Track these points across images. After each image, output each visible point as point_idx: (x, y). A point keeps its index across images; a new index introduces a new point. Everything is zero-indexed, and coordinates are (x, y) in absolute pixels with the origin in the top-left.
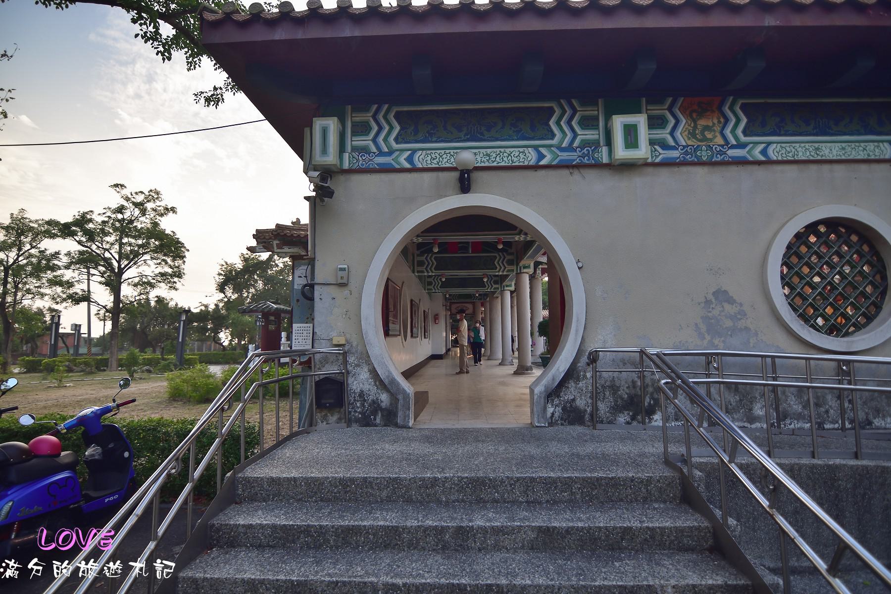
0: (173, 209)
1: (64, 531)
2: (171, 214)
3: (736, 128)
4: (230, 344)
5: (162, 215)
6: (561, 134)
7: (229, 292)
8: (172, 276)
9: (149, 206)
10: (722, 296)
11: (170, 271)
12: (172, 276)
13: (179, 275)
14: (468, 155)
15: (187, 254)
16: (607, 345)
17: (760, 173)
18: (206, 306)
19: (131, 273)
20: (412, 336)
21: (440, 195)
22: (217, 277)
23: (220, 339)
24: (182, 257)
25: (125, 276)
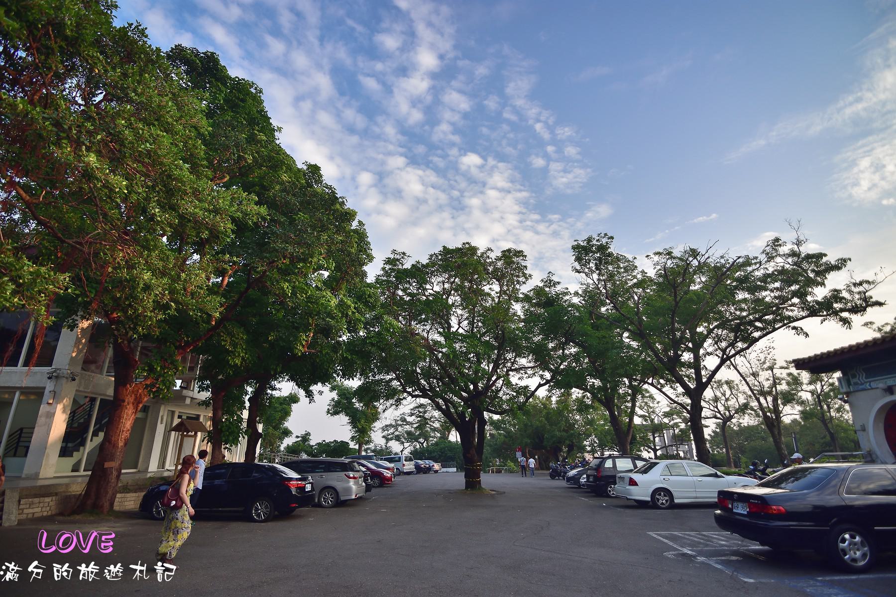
1: (64, 534)
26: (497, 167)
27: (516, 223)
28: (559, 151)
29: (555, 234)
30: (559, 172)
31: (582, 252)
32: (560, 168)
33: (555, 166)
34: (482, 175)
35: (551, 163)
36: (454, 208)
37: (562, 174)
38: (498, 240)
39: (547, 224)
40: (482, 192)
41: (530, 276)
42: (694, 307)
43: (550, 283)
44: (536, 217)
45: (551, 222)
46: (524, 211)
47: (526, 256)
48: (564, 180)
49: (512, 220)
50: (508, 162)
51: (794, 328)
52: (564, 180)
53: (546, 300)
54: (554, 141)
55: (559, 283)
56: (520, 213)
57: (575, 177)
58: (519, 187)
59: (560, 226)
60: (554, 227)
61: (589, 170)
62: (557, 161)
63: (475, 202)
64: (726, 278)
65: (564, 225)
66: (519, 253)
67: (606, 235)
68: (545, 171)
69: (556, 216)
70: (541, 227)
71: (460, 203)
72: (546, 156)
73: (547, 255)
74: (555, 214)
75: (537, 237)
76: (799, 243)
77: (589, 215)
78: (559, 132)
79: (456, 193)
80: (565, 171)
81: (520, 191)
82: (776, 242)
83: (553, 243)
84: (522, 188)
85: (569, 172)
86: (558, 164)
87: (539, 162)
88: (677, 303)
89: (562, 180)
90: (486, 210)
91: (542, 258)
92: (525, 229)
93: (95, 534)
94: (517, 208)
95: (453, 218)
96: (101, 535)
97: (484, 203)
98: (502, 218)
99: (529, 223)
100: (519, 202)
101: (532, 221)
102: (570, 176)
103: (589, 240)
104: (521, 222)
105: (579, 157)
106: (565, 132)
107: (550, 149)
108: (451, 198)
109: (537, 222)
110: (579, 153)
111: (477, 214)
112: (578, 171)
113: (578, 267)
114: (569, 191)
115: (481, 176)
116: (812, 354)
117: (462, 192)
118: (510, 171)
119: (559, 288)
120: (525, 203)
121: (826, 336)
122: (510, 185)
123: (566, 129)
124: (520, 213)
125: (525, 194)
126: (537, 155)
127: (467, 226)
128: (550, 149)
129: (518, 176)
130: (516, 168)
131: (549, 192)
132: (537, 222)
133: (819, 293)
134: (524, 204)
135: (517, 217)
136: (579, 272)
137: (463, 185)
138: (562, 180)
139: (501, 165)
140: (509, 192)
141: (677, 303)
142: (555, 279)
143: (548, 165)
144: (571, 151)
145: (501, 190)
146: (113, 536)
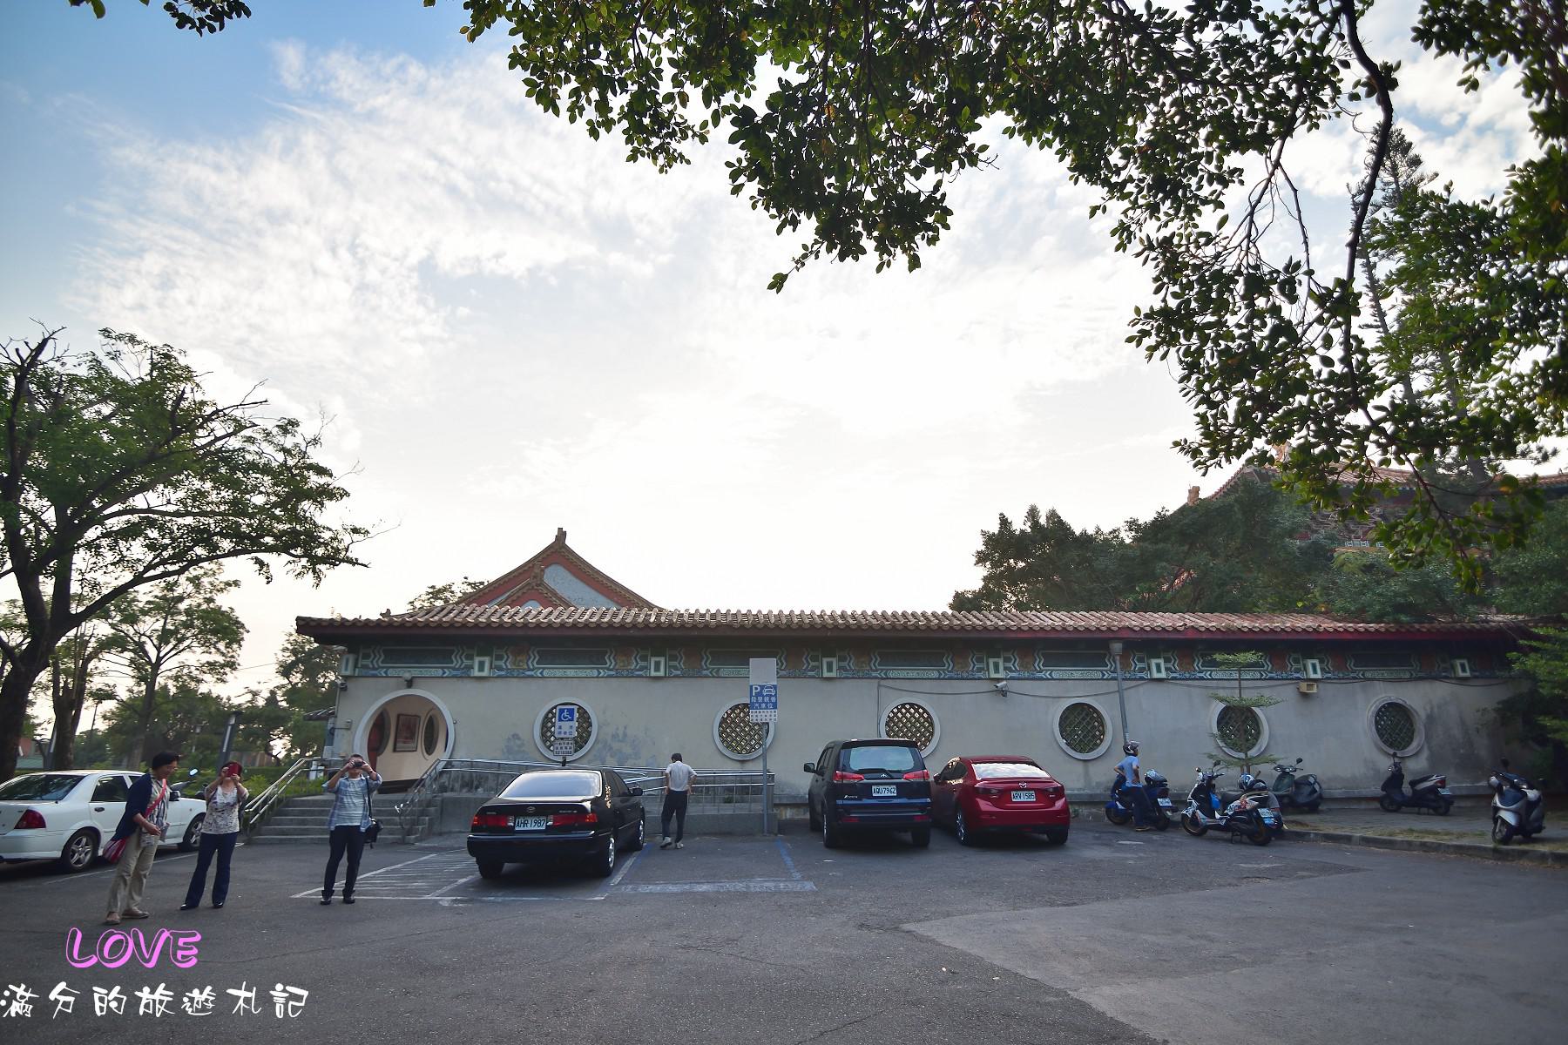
0: (236, 583)
1: (112, 934)
2: (233, 588)
3: (533, 663)
4: (288, 756)
5: (221, 590)
6: (456, 663)
7: (296, 678)
8: (223, 666)
9: (205, 581)
10: (516, 736)
11: (221, 659)
12: (223, 666)
13: (232, 665)
14: (416, 673)
15: (245, 635)
16: (1080, 767)
17: (541, 681)
18: (255, 694)
19: (170, 665)
20: (395, 750)
21: (399, 688)
22: (280, 654)
23: (272, 748)
24: (239, 642)
25: (163, 668)
93: (166, 934)
96: (177, 936)
146: (198, 938)
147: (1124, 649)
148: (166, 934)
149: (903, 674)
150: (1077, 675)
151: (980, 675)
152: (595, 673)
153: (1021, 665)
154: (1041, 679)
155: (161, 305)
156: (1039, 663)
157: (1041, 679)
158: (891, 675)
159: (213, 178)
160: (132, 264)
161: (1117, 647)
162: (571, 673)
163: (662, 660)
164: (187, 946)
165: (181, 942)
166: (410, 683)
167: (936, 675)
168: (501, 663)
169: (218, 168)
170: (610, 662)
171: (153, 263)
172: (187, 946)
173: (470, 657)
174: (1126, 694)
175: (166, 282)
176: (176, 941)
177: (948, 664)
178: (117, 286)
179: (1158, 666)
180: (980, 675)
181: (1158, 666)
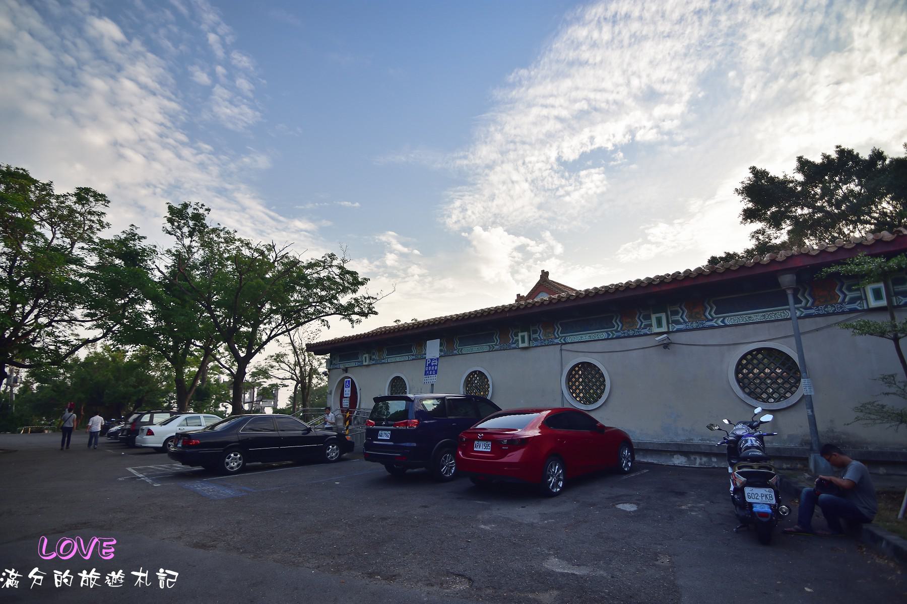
1: (65, 540)
3: (385, 355)
26: (145, 57)
27: (152, 134)
28: (231, 77)
29: (202, 166)
30: (224, 100)
31: (177, 214)
32: (226, 96)
33: (220, 92)
34: (119, 55)
35: (218, 86)
36: (61, 78)
37: (227, 103)
38: (122, 145)
39: (195, 152)
40: (113, 77)
41: (108, 224)
42: (264, 290)
43: (132, 236)
44: (183, 138)
45: (200, 151)
46: (169, 124)
47: (109, 202)
48: (228, 111)
49: (149, 129)
50: (162, 58)
51: (323, 321)
52: (228, 111)
53: (129, 253)
54: (227, 64)
55: (145, 238)
56: (162, 124)
57: (241, 114)
58: (168, 93)
59: (209, 159)
60: (202, 157)
61: (257, 113)
62: (224, 86)
63: (99, 84)
64: (293, 274)
65: (215, 160)
66: (100, 197)
67: (203, 205)
68: (207, 91)
69: (207, 147)
70: (186, 152)
71: (74, 75)
72: (212, 74)
73: (187, 186)
74: (208, 144)
75: (177, 161)
76: (344, 261)
77: (246, 160)
78: (235, 56)
79: (69, 60)
80: (231, 102)
81: (170, 99)
82: (332, 257)
83: (197, 175)
84: (173, 97)
85: (236, 106)
86: (226, 91)
87: (202, 77)
88: (241, 287)
89: (226, 110)
90: (114, 101)
91: (180, 188)
92: (165, 146)
93: (96, 540)
94: (159, 117)
95: (56, 90)
96: (102, 541)
97: (113, 91)
98: (136, 120)
99: (171, 141)
100: (164, 112)
101: (176, 141)
102: (236, 110)
103: (186, 206)
104: (161, 136)
105: (250, 95)
106: (242, 60)
107: (220, 70)
108: (61, 63)
109: (183, 144)
110: (251, 91)
111: (98, 102)
112: (246, 109)
113: (170, 229)
114: (230, 126)
115: (117, 56)
116: (333, 338)
117: (81, 64)
118: (161, 70)
119: (144, 243)
120: (172, 116)
121: (338, 328)
122: (158, 86)
123: (245, 58)
124: (162, 124)
125: (173, 106)
126: (202, 69)
127: (78, 110)
128: (220, 70)
129: (171, 81)
130: (171, 70)
131: (206, 116)
132: (183, 144)
133: (344, 299)
134: (171, 116)
135: (157, 128)
136: (169, 233)
137: (86, 54)
138: (226, 110)
139: (150, 56)
140: (154, 94)
141: (241, 287)
142: (140, 232)
143: (213, 87)
144: (243, 83)
145: (143, 87)
146: (115, 542)
147: (799, 281)
148: (96, 540)
149: (577, 338)
150: (758, 318)
151: (646, 331)
152: (407, 358)
153: (690, 316)
154: (712, 327)
155: (464, 218)
156: (710, 312)
157: (712, 327)
158: (569, 340)
159: (465, 162)
160: (452, 206)
161: (787, 280)
162: (398, 359)
163: (663, 316)
164: (109, 547)
165: (105, 544)
166: (346, 370)
167: (604, 336)
168: (678, 318)
169: (465, 157)
170: (497, 339)
171: (458, 203)
172: (109, 547)
173: (648, 317)
174: (802, 337)
175: (464, 210)
176: (102, 544)
177: (617, 324)
178: (450, 216)
179: (523, 338)
180: (646, 331)
181: (523, 338)
